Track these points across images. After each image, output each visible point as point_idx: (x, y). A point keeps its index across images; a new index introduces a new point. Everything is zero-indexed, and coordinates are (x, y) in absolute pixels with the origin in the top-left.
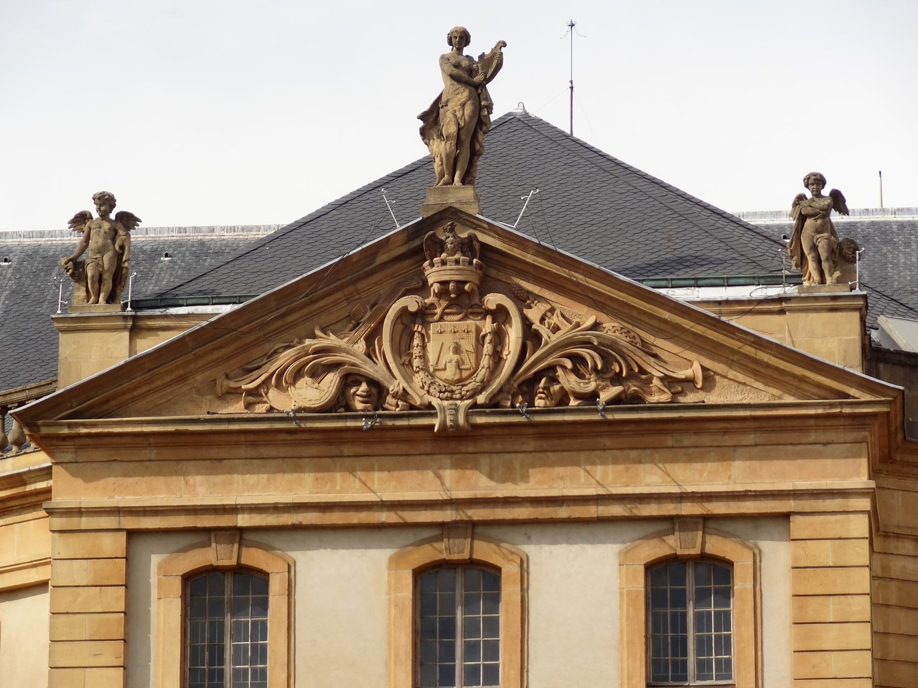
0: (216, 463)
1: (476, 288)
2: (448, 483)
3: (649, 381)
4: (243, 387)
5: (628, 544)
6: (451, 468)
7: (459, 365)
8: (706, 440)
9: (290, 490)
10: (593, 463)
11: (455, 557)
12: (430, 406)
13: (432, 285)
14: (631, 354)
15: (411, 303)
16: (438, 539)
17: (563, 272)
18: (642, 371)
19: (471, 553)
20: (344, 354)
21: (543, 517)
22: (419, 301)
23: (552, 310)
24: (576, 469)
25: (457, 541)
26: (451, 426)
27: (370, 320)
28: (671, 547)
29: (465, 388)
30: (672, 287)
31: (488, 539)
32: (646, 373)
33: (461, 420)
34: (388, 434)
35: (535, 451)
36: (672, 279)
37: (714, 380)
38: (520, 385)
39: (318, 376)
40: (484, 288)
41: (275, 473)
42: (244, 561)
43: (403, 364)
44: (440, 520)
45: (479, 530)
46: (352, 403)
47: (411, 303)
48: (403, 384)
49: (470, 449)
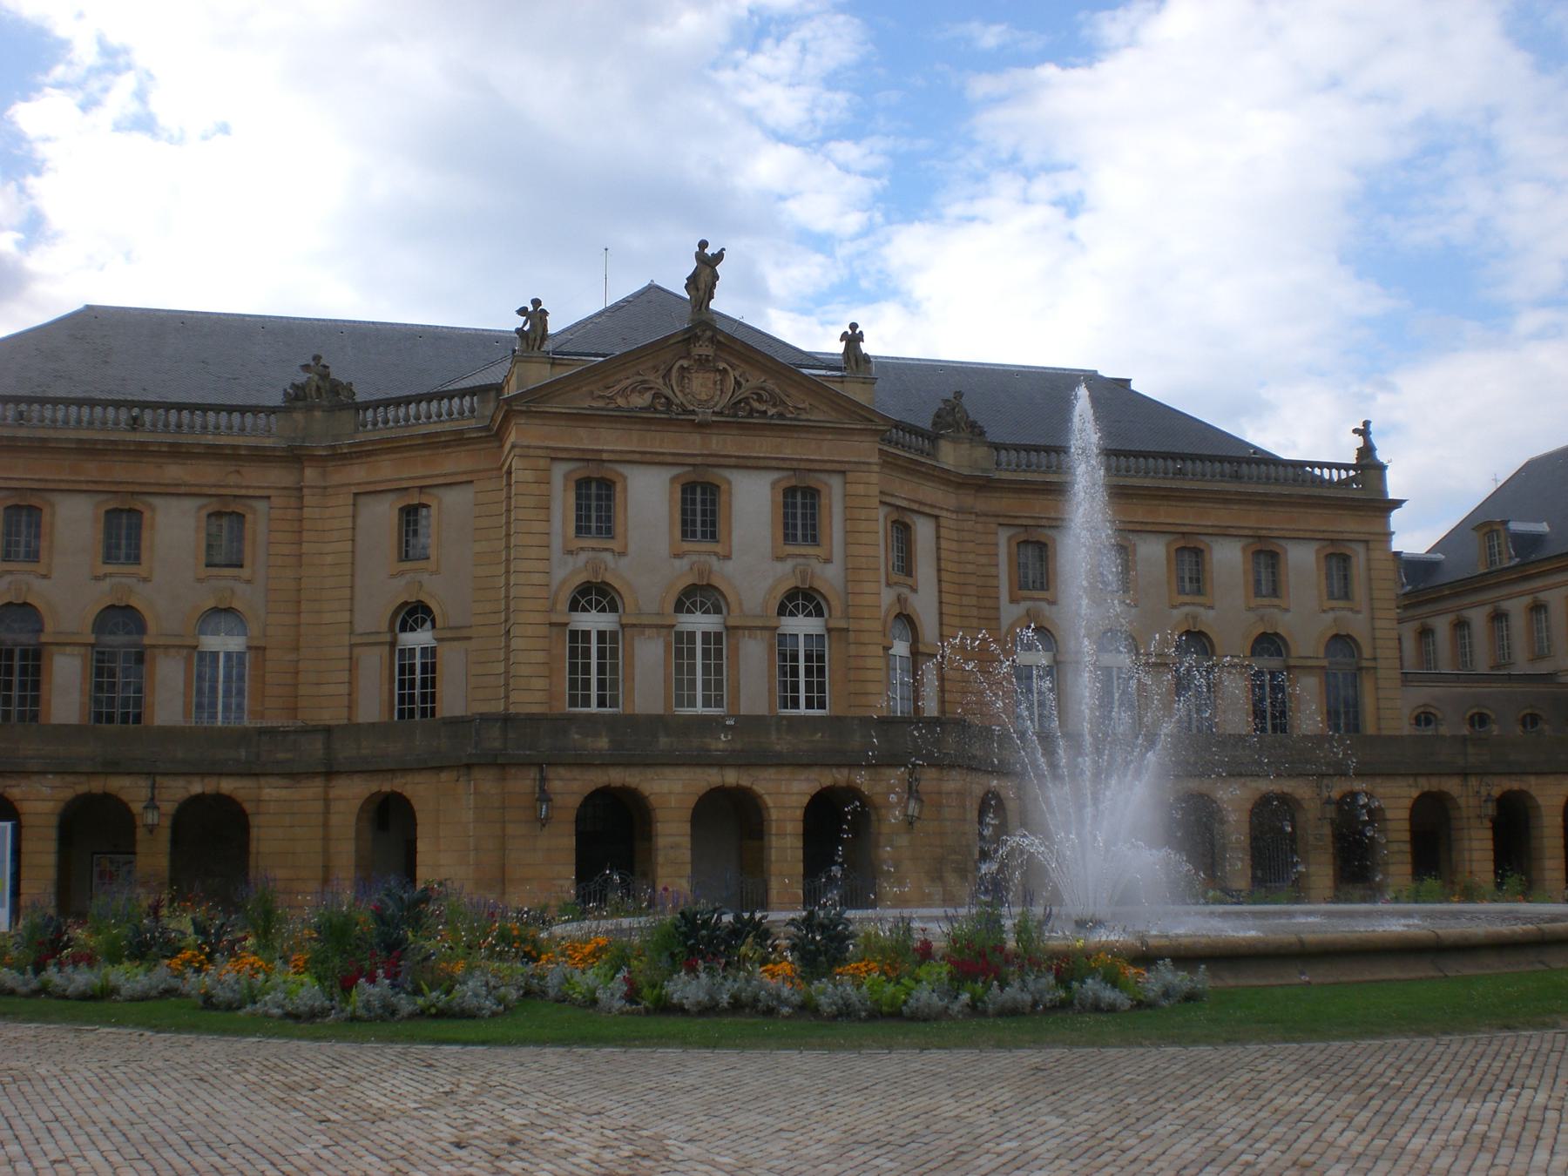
15: (685, 363)
47: (685, 363)
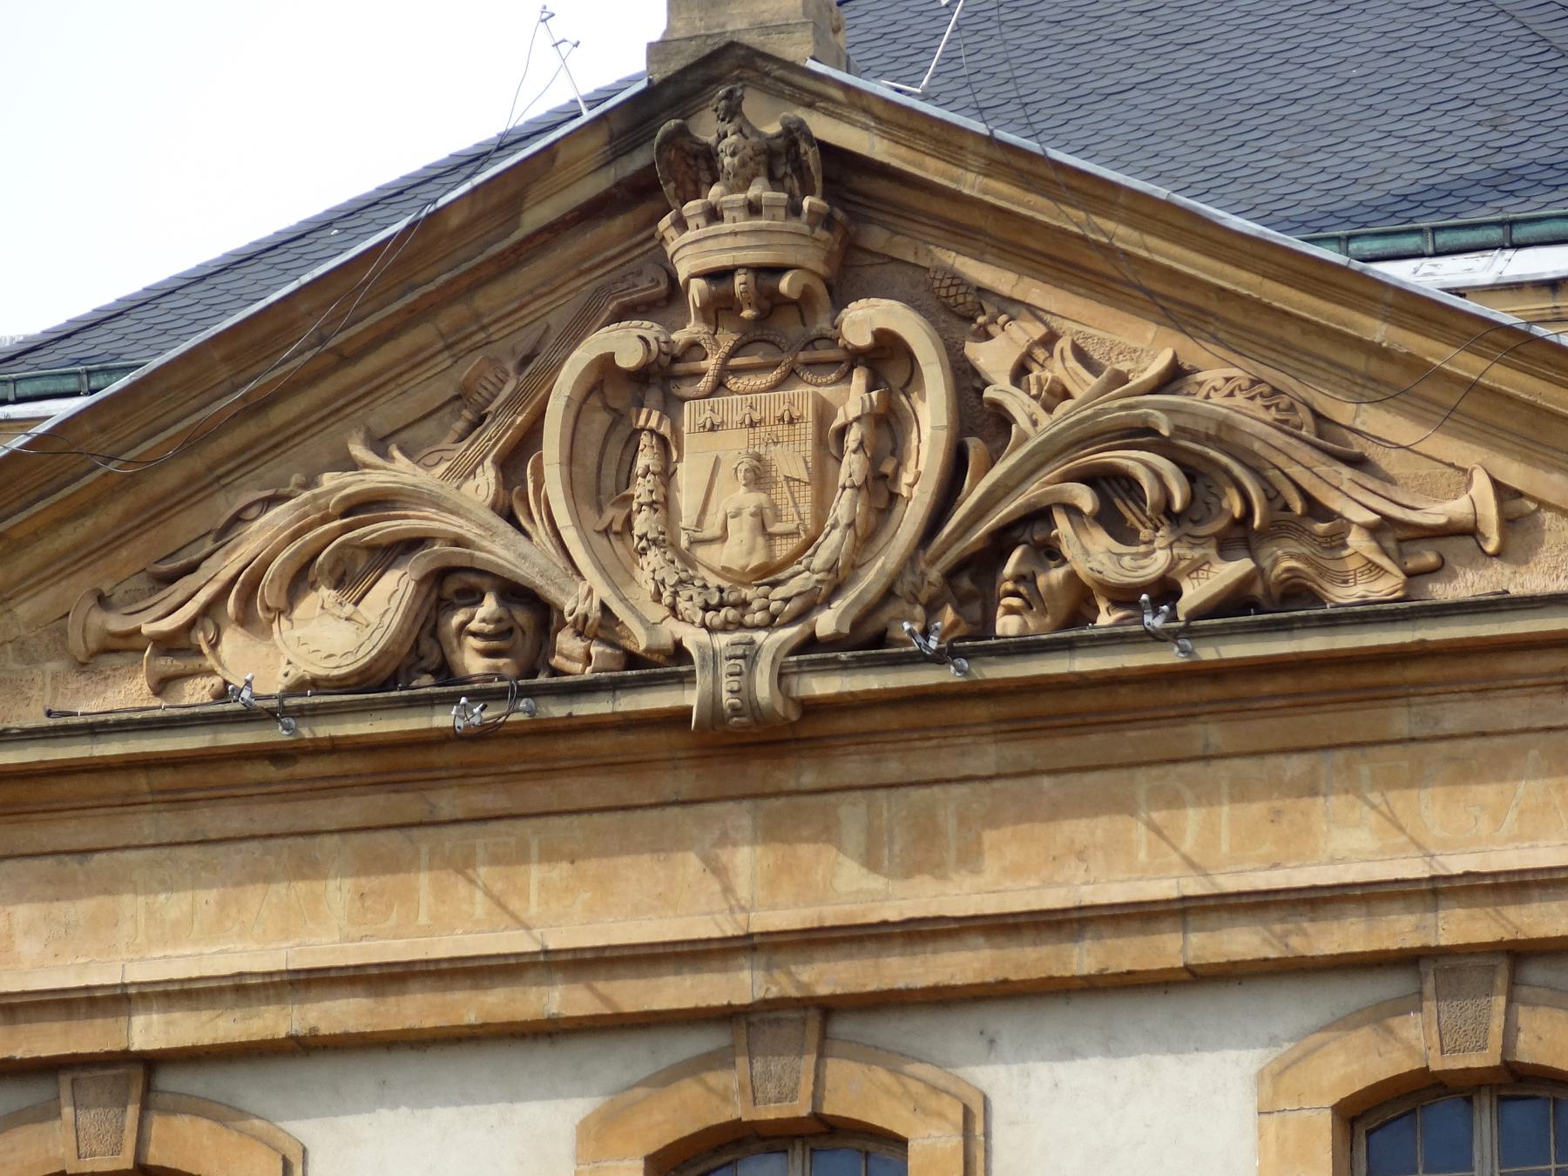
0: (72, 864)
1: (820, 289)
2: (743, 890)
3: (1336, 541)
4: (147, 629)
5: (1287, 1046)
6: (753, 842)
7: (762, 524)
8: (1510, 710)
9: (285, 934)
10: (1174, 802)
11: (770, 1112)
12: (679, 653)
13: (687, 283)
14: (1280, 460)
15: (626, 344)
16: (719, 1060)
17: (1070, 219)
18: (1315, 509)
19: (817, 1097)
20: (429, 512)
21: (1023, 976)
22: (650, 336)
23: (1049, 340)
24: (1121, 821)
25: (776, 1065)
26: (733, 707)
27: (513, 402)
28: (1410, 1049)
29: (780, 592)
30: (1438, 254)
31: (870, 1054)
32: (1327, 514)
33: (763, 688)
34: (562, 746)
35: (997, 776)
36: (1435, 230)
37: (1539, 526)
38: (951, 575)
39: (355, 583)
40: (843, 285)
41: (239, 884)
42: (155, 1157)
43: (606, 532)
44: (719, 1000)
45: (844, 1027)
46: (456, 658)
48: (603, 591)
49: (809, 779)
